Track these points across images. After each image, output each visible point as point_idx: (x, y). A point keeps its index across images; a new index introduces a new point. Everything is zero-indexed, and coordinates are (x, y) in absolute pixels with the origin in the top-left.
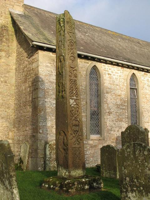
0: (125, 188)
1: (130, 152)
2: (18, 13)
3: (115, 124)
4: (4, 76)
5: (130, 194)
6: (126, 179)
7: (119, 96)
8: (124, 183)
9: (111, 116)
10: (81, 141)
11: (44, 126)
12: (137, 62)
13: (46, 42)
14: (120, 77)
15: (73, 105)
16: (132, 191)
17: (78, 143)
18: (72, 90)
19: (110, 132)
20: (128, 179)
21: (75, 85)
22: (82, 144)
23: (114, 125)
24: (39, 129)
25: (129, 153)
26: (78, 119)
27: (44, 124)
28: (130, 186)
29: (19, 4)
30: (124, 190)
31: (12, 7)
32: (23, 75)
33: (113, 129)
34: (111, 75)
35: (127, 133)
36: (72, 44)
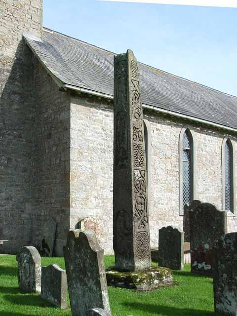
0: (221, 287)
1: (230, 243)
2: (36, 40)
3: (163, 195)
4: (18, 129)
5: (228, 293)
6: (222, 276)
7: (169, 158)
8: (220, 280)
9: (159, 185)
10: (146, 224)
11: (77, 197)
12: (191, 113)
13: (203, 118)
14: (171, 133)
15: (137, 178)
16: (230, 290)
17: (143, 225)
18: (137, 159)
19: (157, 205)
20: (225, 275)
21: (140, 151)
22: (147, 227)
23: (162, 197)
24: (71, 202)
25: (228, 245)
26: (144, 196)
27: (77, 196)
28: (228, 283)
29: (37, 27)
30: (219, 289)
31: (27, 30)
32: (45, 128)
33: (160, 202)
34: (160, 130)
35: (197, 212)
36: (137, 96)
